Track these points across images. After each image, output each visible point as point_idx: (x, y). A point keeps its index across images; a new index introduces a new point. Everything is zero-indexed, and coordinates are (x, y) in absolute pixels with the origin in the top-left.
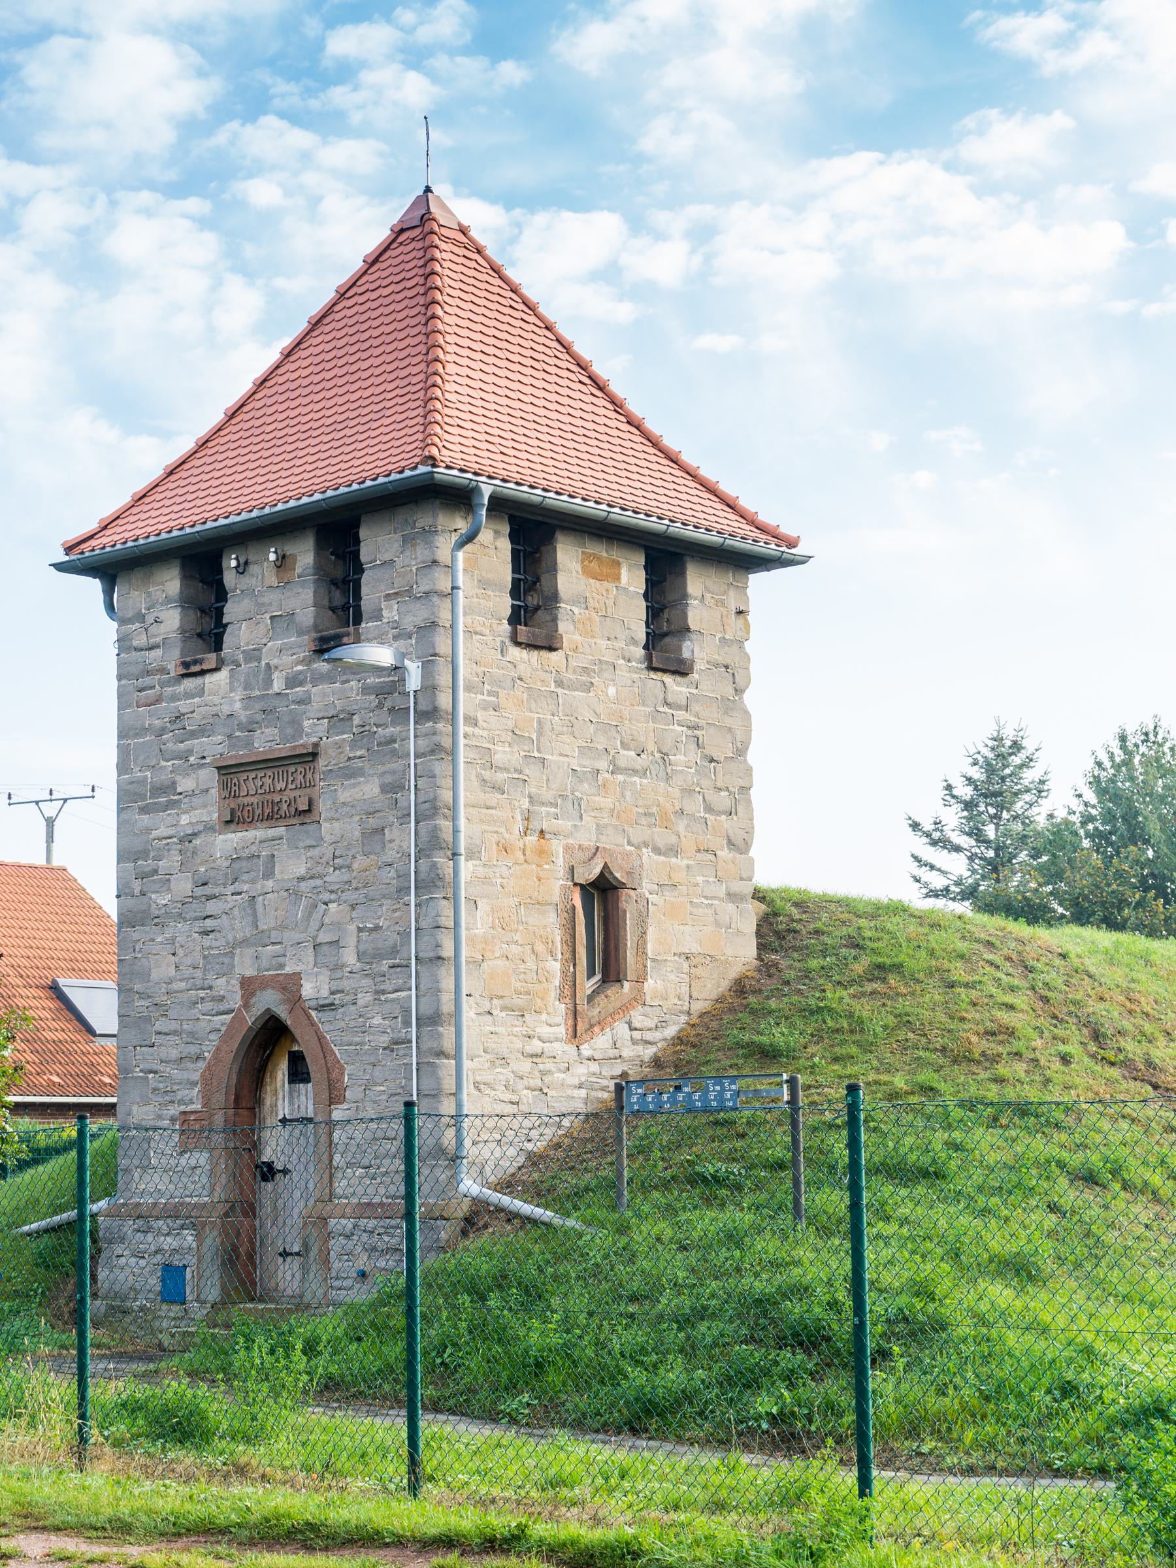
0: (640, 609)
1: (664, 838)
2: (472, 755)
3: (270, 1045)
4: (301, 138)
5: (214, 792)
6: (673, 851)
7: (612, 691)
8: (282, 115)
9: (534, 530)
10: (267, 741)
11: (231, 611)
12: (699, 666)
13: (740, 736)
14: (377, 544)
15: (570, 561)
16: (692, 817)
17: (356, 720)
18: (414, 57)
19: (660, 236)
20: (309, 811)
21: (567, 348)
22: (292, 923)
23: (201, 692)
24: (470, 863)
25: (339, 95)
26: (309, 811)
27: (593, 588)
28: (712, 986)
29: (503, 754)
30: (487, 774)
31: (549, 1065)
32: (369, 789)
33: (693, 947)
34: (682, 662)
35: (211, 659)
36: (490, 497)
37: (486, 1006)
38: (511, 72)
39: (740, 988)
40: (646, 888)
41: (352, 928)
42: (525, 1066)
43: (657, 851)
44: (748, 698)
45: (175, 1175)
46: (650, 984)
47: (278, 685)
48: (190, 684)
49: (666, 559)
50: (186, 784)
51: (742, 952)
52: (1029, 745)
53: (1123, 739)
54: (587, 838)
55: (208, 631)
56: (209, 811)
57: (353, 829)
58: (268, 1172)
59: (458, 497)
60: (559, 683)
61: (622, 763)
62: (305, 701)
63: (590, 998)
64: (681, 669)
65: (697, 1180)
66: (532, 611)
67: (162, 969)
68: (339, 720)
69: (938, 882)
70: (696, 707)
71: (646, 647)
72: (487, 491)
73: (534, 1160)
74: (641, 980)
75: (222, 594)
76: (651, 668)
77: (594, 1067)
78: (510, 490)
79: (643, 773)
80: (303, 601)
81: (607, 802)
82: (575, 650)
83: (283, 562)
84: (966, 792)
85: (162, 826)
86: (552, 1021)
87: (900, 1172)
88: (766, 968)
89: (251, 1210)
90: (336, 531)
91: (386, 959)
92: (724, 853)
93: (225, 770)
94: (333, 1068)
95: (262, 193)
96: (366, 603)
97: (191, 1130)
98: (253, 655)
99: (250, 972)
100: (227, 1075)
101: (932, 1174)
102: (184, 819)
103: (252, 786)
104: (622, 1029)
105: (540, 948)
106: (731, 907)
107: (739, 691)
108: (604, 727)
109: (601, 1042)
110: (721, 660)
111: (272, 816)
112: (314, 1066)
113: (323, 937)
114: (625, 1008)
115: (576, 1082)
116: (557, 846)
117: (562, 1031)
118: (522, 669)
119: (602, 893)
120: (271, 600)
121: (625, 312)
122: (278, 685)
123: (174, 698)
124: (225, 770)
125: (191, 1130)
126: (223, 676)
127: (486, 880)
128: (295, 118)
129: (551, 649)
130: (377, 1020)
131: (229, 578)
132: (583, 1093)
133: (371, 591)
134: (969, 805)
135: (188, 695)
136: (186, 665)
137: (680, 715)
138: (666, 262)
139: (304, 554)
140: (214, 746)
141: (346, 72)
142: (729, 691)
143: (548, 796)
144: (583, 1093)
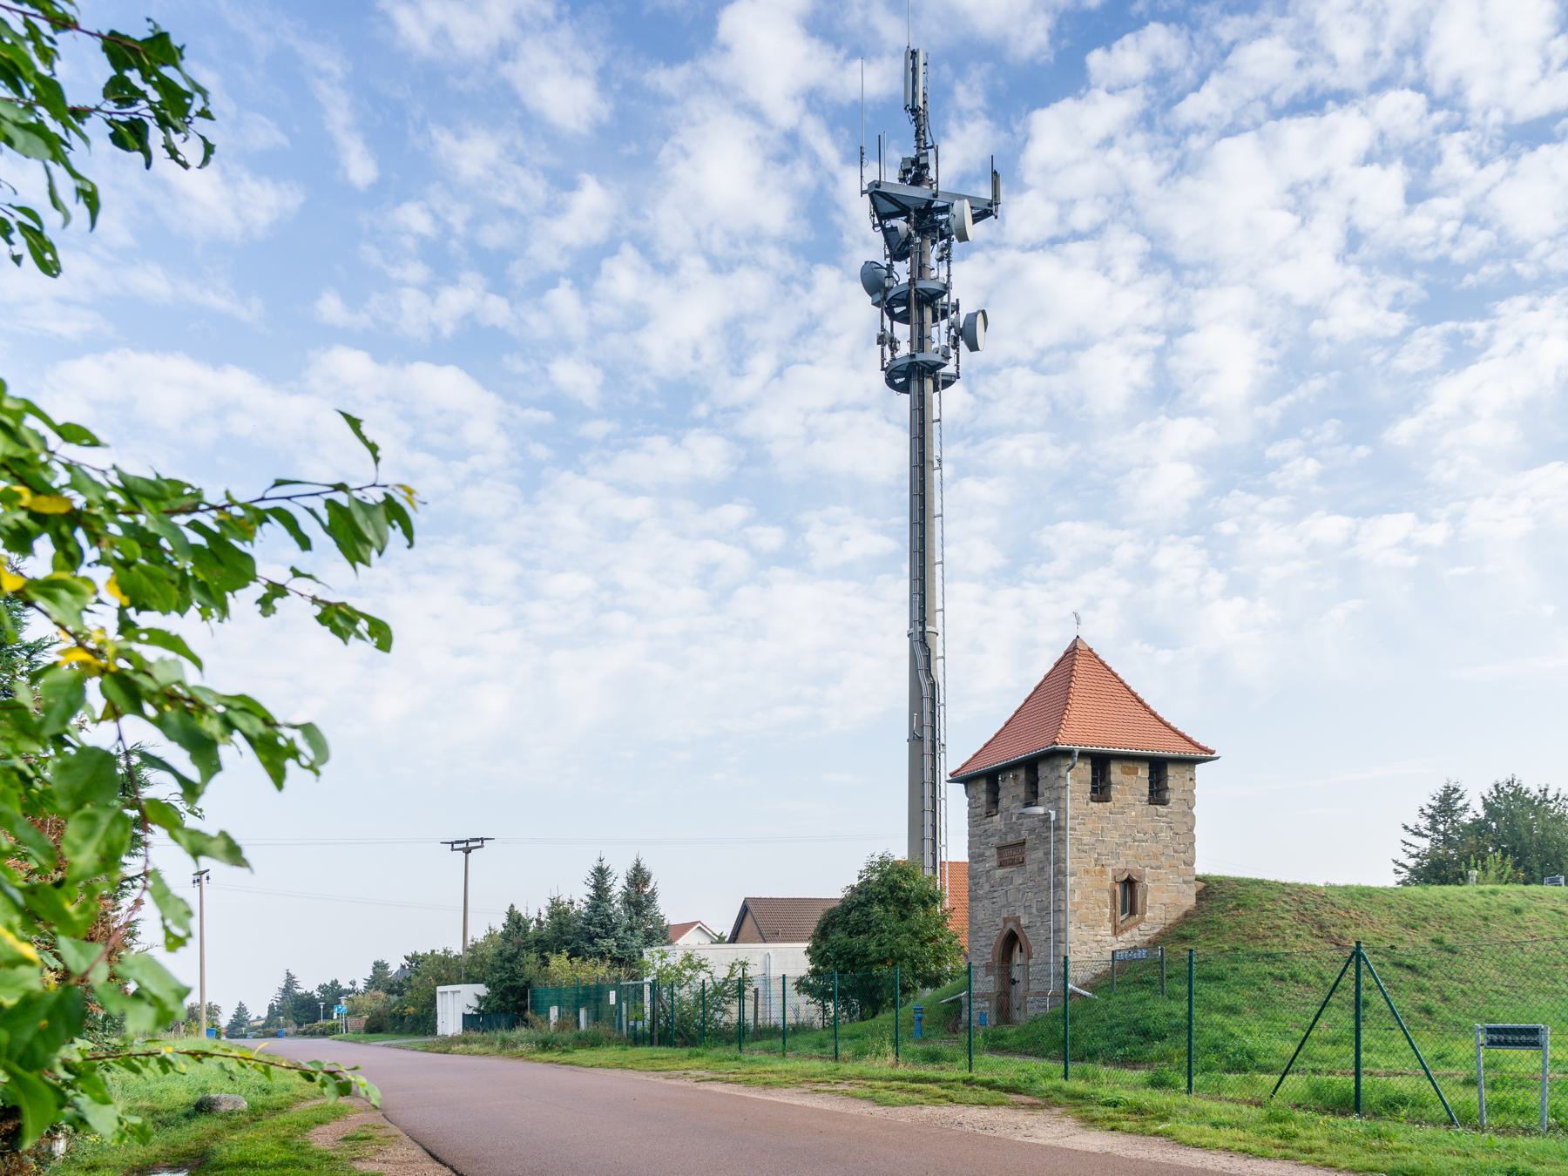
1: (1154, 863)
3: (1011, 941)
4: (1251, 499)
8: (1242, 489)
9: (1101, 763)
10: (1011, 839)
11: (1001, 794)
14: (1043, 771)
15: (1116, 772)
18: (1310, 451)
19: (1432, 521)
21: (1128, 689)
22: (1016, 900)
25: (1272, 477)
27: (1126, 778)
28: (1174, 915)
29: (1086, 839)
32: (1040, 854)
38: (1362, 451)
39: (1186, 914)
44: (1195, 810)
45: (985, 983)
49: (1158, 767)
50: (988, 853)
51: (1190, 902)
52: (1462, 789)
53: (1496, 786)
54: (1121, 866)
55: (994, 801)
57: (1035, 867)
58: (1014, 982)
59: (1068, 754)
64: (1164, 803)
65: (1141, 982)
66: (1100, 789)
67: (981, 916)
68: (1032, 831)
69: (1414, 851)
73: (1097, 976)
74: (1144, 913)
75: (998, 789)
80: (1021, 791)
83: (1015, 777)
84: (1430, 811)
85: (980, 867)
86: (1106, 930)
87: (1208, 978)
88: (1198, 907)
89: (1008, 994)
90: (1031, 766)
91: (1044, 910)
94: (1029, 947)
95: (1228, 528)
97: (989, 968)
98: (1007, 809)
100: (999, 950)
101: (1219, 978)
103: (1007, 853)
104: (1135, 931)
108: (1129, 827)
109: (1127, 935)
111: (1012, 864)
116: (1109, 870)
119: (1129, 884)
120: (1013, 789)
121: (1413, 561)
125: (989, 968)
128: (1248, 490)
133: (1041, 789)
134: (1432, 817)
138: (1436, 534)
139: (1022, 775)
140: (995, 840)
141: (1276, 465)
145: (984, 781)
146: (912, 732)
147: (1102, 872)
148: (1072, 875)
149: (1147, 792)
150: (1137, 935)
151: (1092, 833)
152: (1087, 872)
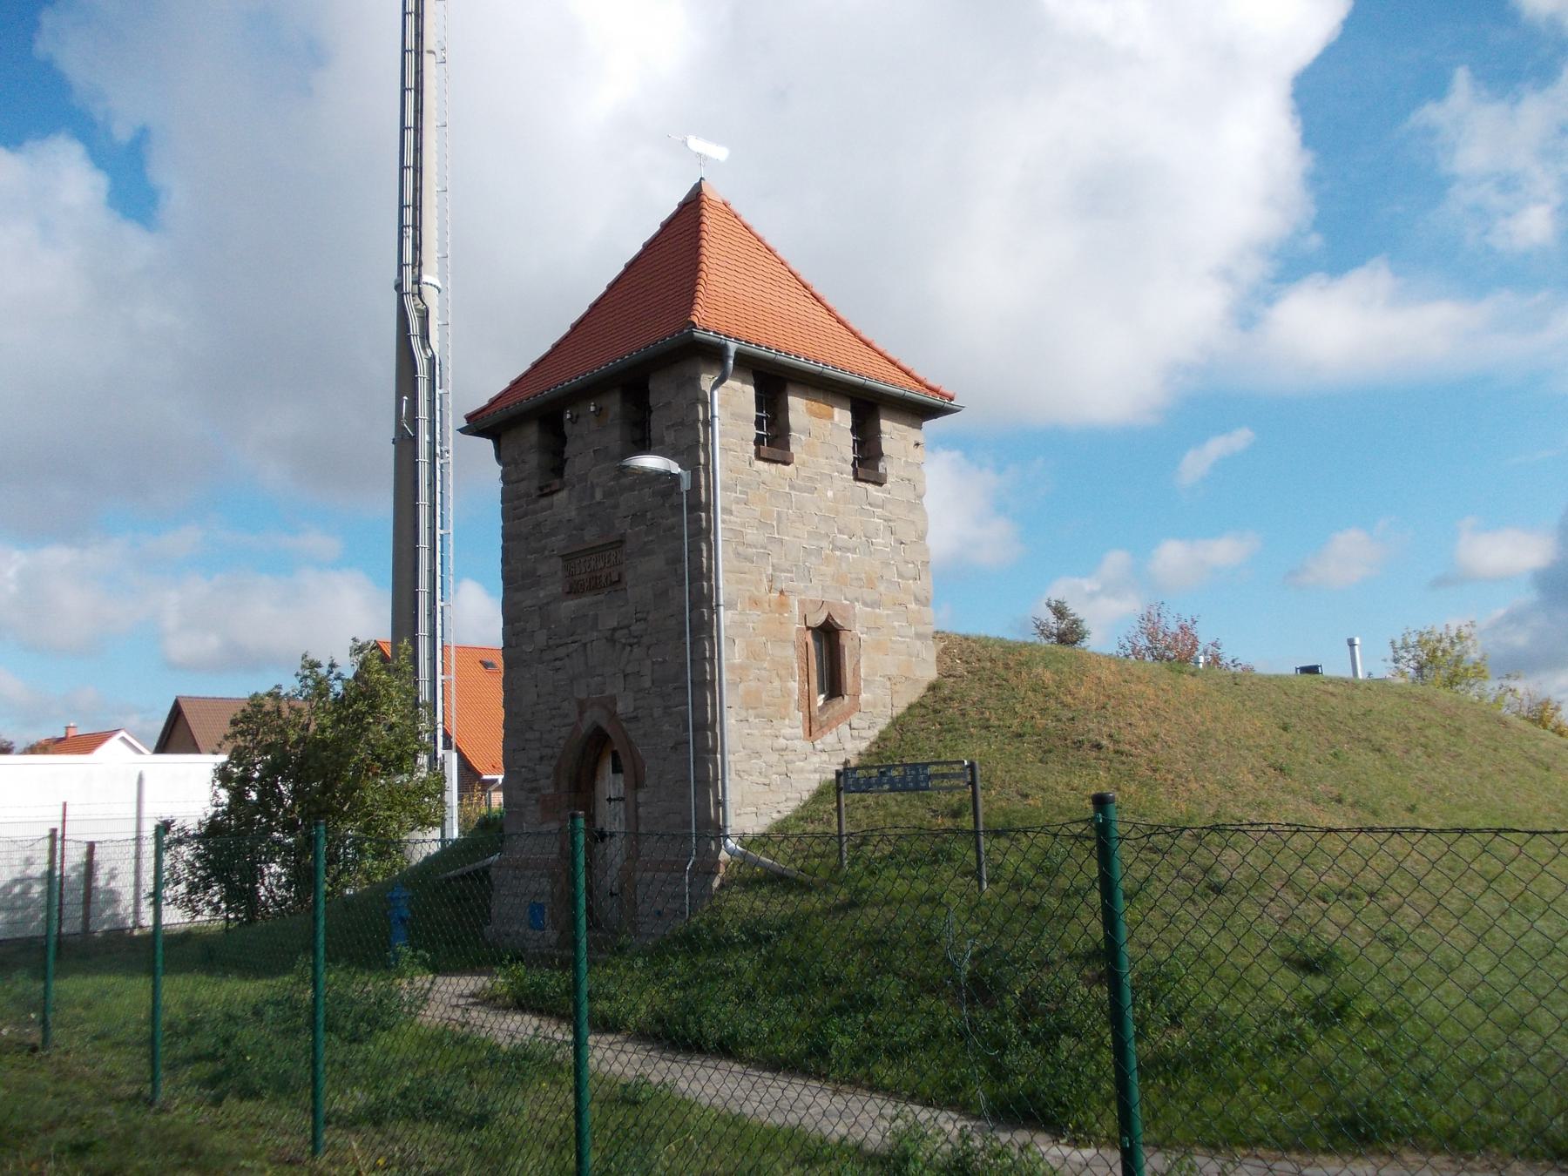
0: (849, 438)
1: (870, 596)
2: (730, 535)
5: (560, 574)
6: (875, 604)
7: (830, 494)
9: (774, 382)
10: (591, 536)
11: (569, 450)
12: (890, 479)
13: (751, 1052)
14: (660, 390)
15: (798, 407)
16: (890, 581)
17: (649, 515)
20: (619, 581)
23: (551, 507)
24: (730, 613)
26: (619, 581)
28: (911, 695)
29: (752, 534)
30: (740, 549)
31: (791, 756)
33: (893, 672)
34: (880, 475)
35: (557, 483)
36: (737, 353)
37: (744, 714)
40: (858, 630)
41: (648, 662)
42: (775, 757)
43: (865, 604)
46: (864, 696)
47: (598, 496)
48: (544, 502)
49: (869, 408)
50: (542, 569)
54: (815, 595)
55: (556, 466)
56: (557, 588)
60: (792, 487)
61: (839, 544)
62: (616, 506)
63: (821, 709)
64: (879, 481)
66: (773, 438)
68: (637, 517)
70: (889, 507)
71: (853, 465)
72: (733, 346)
74: (856, 695)
75: (563, 439)
76: (857, 479)
77: (825, 757)
78: (752, 349)
79: (854, 550)
81: (830, 570)
82: (803, 464)
92: (912, 606)
93: (567, 558)
96: (654, 434)
99: (583, 696)
102: (542, 594)
104: (844, 728)
105: (783, 672)
106: (918, 643)
107: (920, 497)
109: (830, 738)
110: (906, 475)
111: (594, 585)
112: (625, 762)
113: (629, 670)
114: (849, 714)
115: (812, 767)
117: (800, 732)
118: (765, 476)
119: (828, 636)
120: (590, 432)
122: (598, 496)
123: (535, 512)
124: (567, 558)
126: (563, 495)
127: (742, 624)
129: (786, 463)
130: (666, 727)
131: (568, 428)
132: (817, 776)
135: (544, 509)
136: (541, 489)
137: (879, 511)
139: (614, 404)
140: (558, 542)
142: (912, 497)
143: (787, 565)
144: (817, 776)
145: (528, 423)
146: (399, 428)
147: (783, 605)
148: (730, 606)
149: (850, 456)
150: (851, 739)
151: (762, 524)
152: (756, 603)
